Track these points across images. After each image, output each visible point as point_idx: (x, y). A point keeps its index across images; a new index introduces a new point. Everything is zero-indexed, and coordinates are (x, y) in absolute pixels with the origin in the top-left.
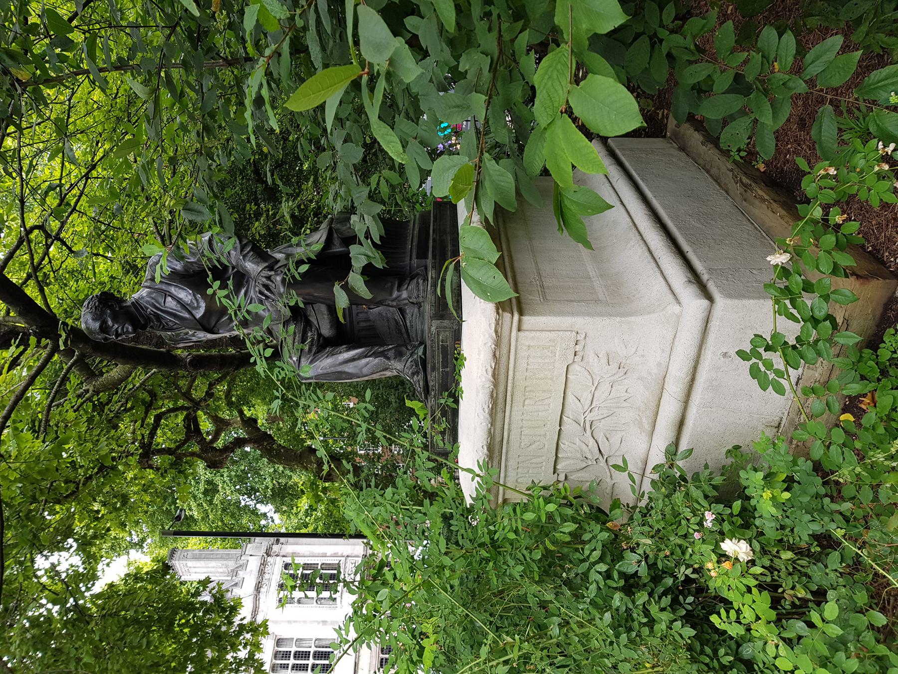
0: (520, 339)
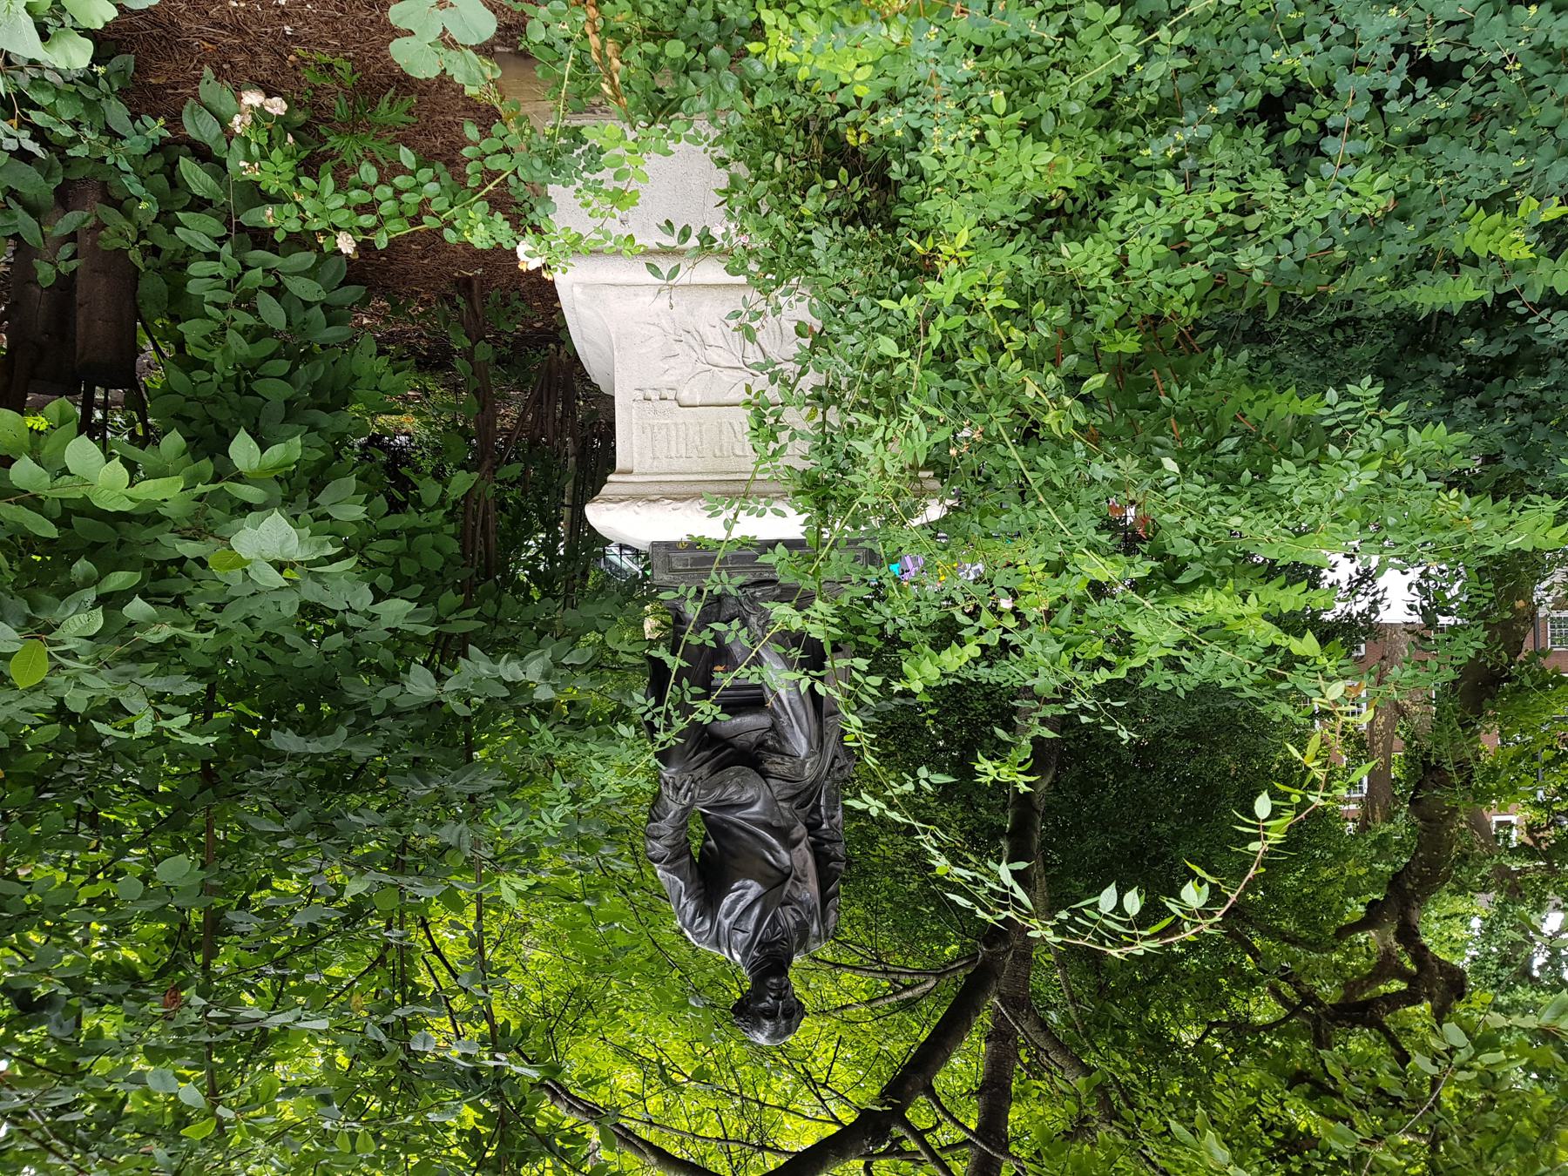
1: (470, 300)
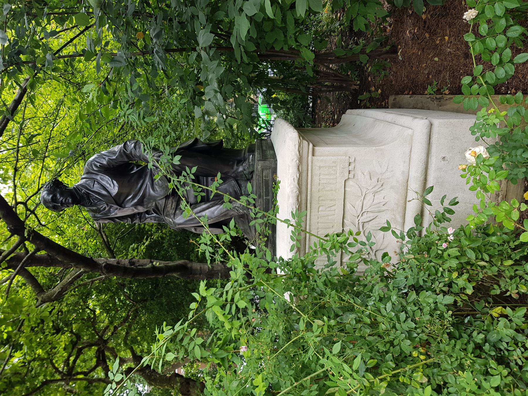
0: (314, 162)
1: (387, 52)
